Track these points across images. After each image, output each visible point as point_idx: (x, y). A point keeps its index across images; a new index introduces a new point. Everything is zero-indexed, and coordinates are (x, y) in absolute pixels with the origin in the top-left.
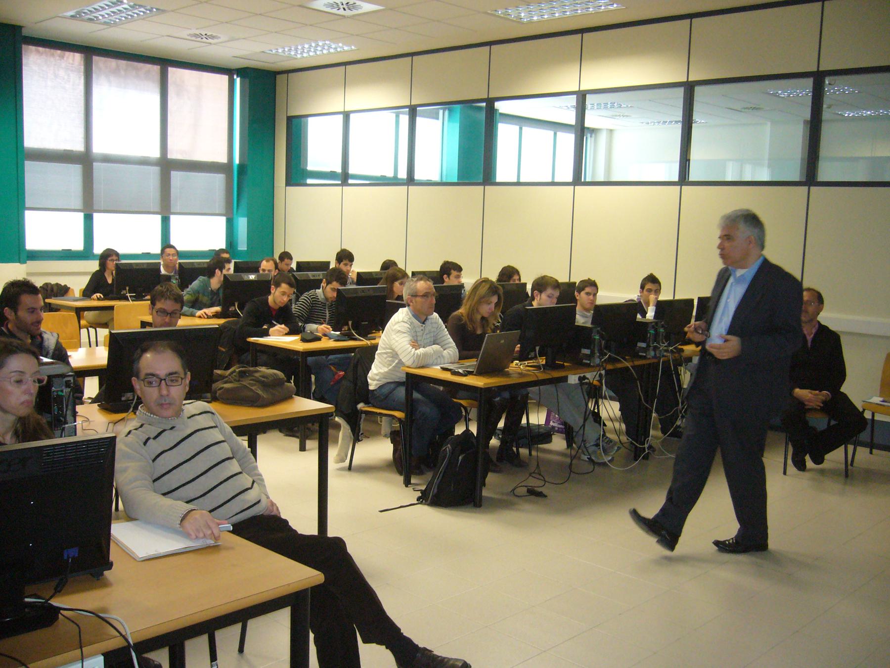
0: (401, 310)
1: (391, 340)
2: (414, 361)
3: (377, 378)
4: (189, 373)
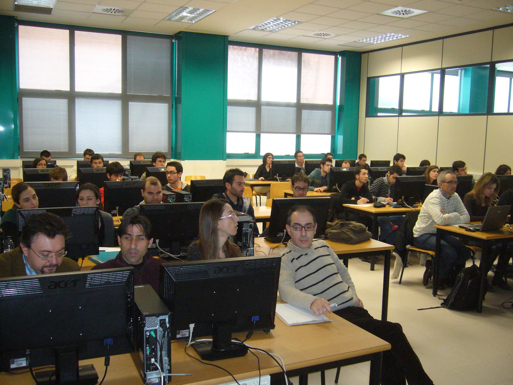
0: (434, 190)
1: (428, 208)
2: (442, 222)
3: (419, 230)
4: (316, 224)
